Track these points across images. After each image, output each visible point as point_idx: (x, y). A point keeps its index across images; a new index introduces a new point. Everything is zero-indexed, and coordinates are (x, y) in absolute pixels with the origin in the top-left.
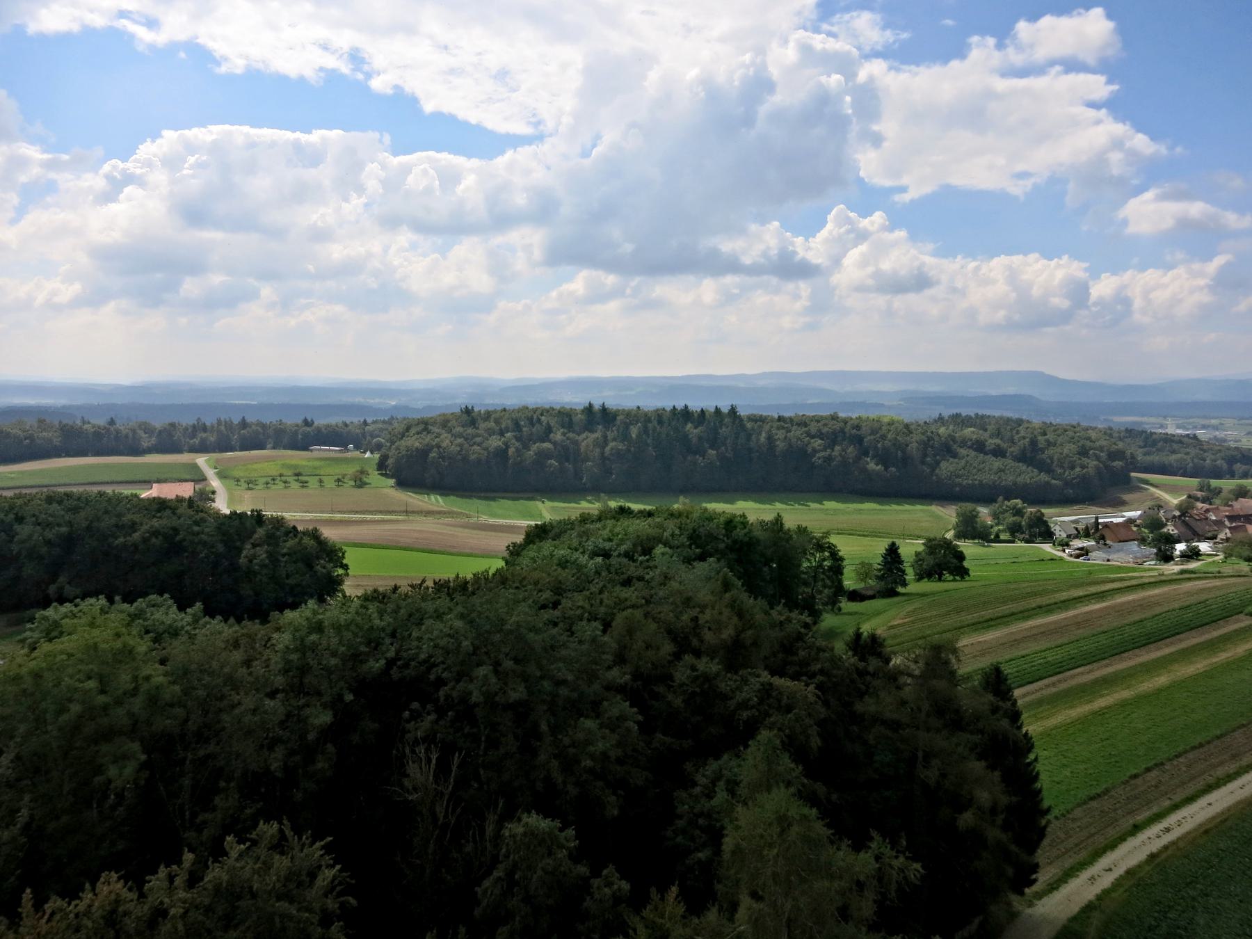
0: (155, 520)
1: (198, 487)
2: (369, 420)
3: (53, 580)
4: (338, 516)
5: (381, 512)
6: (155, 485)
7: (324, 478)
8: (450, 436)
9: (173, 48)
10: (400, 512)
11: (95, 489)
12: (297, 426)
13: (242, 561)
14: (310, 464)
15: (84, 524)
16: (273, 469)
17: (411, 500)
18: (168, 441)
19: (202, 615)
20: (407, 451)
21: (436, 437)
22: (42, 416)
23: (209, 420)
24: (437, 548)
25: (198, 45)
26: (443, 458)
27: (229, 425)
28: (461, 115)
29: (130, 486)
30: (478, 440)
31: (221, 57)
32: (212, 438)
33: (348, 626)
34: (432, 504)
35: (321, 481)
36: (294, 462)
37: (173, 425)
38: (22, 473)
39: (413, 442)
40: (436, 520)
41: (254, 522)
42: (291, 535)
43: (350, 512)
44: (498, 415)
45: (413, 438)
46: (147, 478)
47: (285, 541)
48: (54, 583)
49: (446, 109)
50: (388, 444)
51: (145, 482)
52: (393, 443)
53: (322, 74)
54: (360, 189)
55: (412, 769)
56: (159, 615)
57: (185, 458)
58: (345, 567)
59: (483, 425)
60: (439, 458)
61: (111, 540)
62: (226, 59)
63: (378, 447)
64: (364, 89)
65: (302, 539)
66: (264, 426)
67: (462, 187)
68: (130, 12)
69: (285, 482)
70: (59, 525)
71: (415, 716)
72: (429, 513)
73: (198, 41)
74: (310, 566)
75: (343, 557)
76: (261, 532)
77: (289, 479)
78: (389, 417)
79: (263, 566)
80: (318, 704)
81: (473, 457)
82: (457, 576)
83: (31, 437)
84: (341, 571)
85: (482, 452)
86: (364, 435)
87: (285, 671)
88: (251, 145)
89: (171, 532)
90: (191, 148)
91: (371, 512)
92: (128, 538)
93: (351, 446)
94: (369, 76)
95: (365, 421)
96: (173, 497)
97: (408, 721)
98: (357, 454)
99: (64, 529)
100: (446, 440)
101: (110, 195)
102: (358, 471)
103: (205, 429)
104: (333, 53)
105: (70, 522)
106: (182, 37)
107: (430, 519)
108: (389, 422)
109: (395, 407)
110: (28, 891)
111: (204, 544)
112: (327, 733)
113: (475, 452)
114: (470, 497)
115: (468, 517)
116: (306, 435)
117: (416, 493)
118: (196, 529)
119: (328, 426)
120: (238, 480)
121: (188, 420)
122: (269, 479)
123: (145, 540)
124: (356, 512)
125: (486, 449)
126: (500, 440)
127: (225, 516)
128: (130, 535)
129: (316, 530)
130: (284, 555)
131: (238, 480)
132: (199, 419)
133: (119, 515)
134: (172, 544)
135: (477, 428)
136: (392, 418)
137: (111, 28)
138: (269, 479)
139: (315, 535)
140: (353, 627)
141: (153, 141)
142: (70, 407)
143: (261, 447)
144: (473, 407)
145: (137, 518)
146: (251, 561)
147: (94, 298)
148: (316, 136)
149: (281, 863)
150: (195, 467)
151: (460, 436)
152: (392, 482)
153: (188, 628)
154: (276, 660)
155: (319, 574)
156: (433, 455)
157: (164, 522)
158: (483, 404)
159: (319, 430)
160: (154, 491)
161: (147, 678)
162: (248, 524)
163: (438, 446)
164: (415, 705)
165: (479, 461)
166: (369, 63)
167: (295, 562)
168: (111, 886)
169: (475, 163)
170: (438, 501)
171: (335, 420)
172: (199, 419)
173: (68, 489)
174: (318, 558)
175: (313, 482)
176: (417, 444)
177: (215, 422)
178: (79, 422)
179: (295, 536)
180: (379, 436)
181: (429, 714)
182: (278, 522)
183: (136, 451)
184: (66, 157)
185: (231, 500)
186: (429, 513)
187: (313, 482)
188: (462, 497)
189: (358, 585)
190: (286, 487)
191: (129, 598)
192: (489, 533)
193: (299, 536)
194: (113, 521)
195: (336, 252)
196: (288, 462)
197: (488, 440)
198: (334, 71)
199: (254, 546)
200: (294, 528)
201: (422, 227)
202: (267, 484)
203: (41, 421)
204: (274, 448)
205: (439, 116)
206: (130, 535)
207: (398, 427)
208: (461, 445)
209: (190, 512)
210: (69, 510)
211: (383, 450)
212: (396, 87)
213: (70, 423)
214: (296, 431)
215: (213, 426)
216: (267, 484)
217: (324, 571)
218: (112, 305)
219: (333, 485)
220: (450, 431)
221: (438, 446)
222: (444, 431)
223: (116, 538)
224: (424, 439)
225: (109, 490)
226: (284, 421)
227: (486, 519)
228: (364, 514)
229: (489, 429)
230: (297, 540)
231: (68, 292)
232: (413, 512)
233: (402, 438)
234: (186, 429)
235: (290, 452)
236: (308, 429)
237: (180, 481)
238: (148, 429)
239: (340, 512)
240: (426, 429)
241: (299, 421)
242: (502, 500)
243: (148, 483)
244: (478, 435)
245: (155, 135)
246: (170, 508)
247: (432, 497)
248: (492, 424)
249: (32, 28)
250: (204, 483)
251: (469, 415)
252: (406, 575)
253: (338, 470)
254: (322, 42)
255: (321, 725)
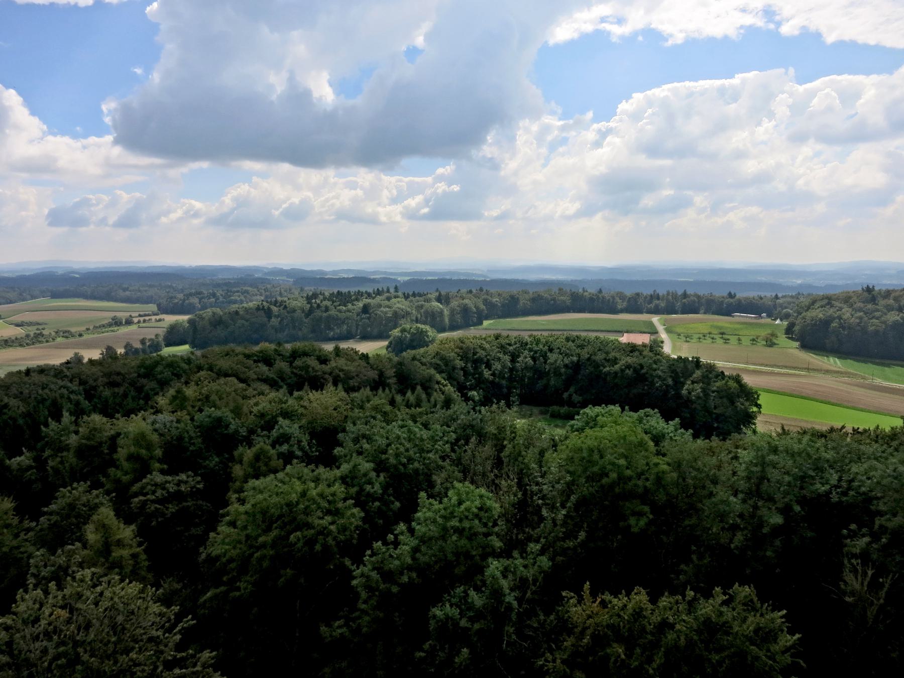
0: (628, 358)
1: (653, 337)
2: (780, 295)
3: (566, 390)
4: (752, 367)
5: (786, 367)
6: (625, 334)
7: (742, 338)
8: (850, 310)
9: (635, 34)
10: (803, 368)
11: (593, 335)
12: (723, 297)
13: (684, 392)
14: (731, 326)
15: (587, 356)
16: (704, 328)
17: (811, 360)
18: (634, 305)
19: (679, 427)
20: (812, 321)
21: (838, 310)
22: (560, 286)
23: (662, 292)
24: (832, 401)
25: (653, 30)
26: (844, 328)
27: (675, 296)
28: (861, 40)
29: (615, 334)
30: (877, 314)
31: (668, 34)
32: (663, 304)
33: (800, 454)
34: (831, 365)
35: (739, 340)
36: (720, 324)
37: (638, 294)
38: (549, 321)
39: (818, 313)
40: (834, 379)
41: (694, 365)
42: (720, 377)
43: (761, 365)
44: (897, 294)
45: (817, 311)
46: (620, 330)
47: (715, 382)
48: (567, 391)
49: (847, 37)
50: (795, 314)
51: (619, 332)
52: (799, 313)
53: (742, 31)
54: (771, 115)
55: (849, 577)
56: (653, 422)
57: (644, 317)
58: (759, 406)
59: (882, 302)
60: (839, 328)
61: (602, 368)
62: (671, 36)
63: (786, 316)
64: (775, 35)
65: (727, 381)
66: (698, 297)
67: (862, 101)
68: (607, 17)
69: (713, 339)
70: (572, 355)
71: (853, 535)
72: (827, 372)
73: (652, 26)
74: (732, 403)
75: (758, 399)
76: (698, 374)
77: (715, 336)
78: (797, 293)
79: (698, 398)
80: (774, 508)
81: (871, 328)
82: (878, 427)
83: (554, 300)
84: (755, 409)
85: (880, 324)
86: (775, 306)
87: (749, 478)
88: (691, 95)
89: (639, 367)
90: (650, 103)
91: (778, 367)
92: (612, 368)
93: (764, 315)
94: (779, 24)
95: (777, 295)
96: (640, 343)
97: (846, 538)
98: (769, 320)
99: (575, 359)
100: (847, 313)
101: (598, 144)
102: (768, 334)
103: (658, 298)
104: (751, 13)
105: (579, 354)
106: (640, 25)
107: (829, 376)
108: (797, 297)
109: (800, 286)
110: (588, 583)
111: (659, 377)
112: (776, 530)
113: (873, 325)
114: (865, 362)
115: (864, 378)
116: (730, 305)
117: (816, 354)
118: (655, 366)
119: (746, 299)
120: (679, 335)
121: (647, 291)
122: (701, 336)
123: (622, 371)
124: (767, 366)
125: (884, 322)
126: (898, 315)
127: (674, 359)
128: (613, 366)
129: (738, 376)
130: (713, 392)
131: (679, 335)
132: (655, 291)
133: (607, 353)
134: (640, 376)
135: (877, 305)
136: (799, 294)
137: (597, 30)
138: (701, 336)
139: (737, 379)
140: (803, 455)
141: (627, 102)
142: (576, 281)
143: (696, 312)
144: (873, 287)
145: (618, 355)
146: (690, 393)
147: (588, 211)
148: (737, 80)
149: (752, 621)
150: (651, 324)
151: (860, 310)
152: (797, 344)
153: (672, 435)
154: (741, 470)
155: (739, 409)
156: (834, 325)
157: (635, 359)
158: (883, 283)
159: (739, 301)
160: (625, 339)
161: (657, 465)
162: (689, 367)
163: (840, 318)
164: (853, 527)
165: (876, 332)
166: (779, 14)
167: (721, 398)
168: (640, 597)
169: (874, 78)
170: (835, 362)
171: (752, 294)
172: (655, 291)
173: (578, 333)
174: (739, 397)
175: (733, 340)
176: (821, 316)
177: (665, 293)
178: (581, 290)
179: (723, 379)
180: (786, 308)
181: (863, 536)
182: (711, 368)
183: (614, 311)
184: (571, 122)
185: (674, 348)
186: (827, 372)
187: (733, 340)
188: (858, 361)
189: (767, 422)
190: (713, 342)
191: (634, 409)
192: (883, 394)
193: (726, 378)
194: (604, 356)
195: (751, 167)
196: (715, 324)
197: (886, 314)
198: (751, 26)
199: (693, 382)
200: (722, 373)
201: (828, 138)
202: (700, 338)
203: (560, 290)
204: (705, 313)
205: (841, 45)
206: (613, 366)
207: (806, 301)
208: (861, 318)
209: (651, 354)
210: (578, 346)
211: (791, 319)
212: (804, 27)
213: (576, 291)
214: (722, 301)
215: (663, 295)
216: (700, 338)
217: (743, 407)
218: (599, 216)
219: (749, 343)
220: (851, 306)
221: (840, 318)
222: (845, 306)
223: (605, 367)
224: (827, 312)
225: (602, 335)
226: (714, 294)
227: (878, 381)
228: (772, 367)
229: (888, 305)
230: (724, 382)
231: (573, 208)
232: (814, 370)
233: (807, 310)
234: (646, 297)
235: (716, 317)
236: (731, 300)
237: (641, 332)
238: (622, 296)
239: (754, 364)
240: (829, 303)
241: (725, 294)
242: (897, 367)
243: (621, 332)
244: (878, 310)
245: (628, 97)
246: (639, 350)
247: (831, 359)
248: (891, 302)
249: (551, 42)
250: (656, 335)
251: (870, 294)
252: (806, 419)
253: (754, 332)
254: (741, 7)
255: (775, 524)
